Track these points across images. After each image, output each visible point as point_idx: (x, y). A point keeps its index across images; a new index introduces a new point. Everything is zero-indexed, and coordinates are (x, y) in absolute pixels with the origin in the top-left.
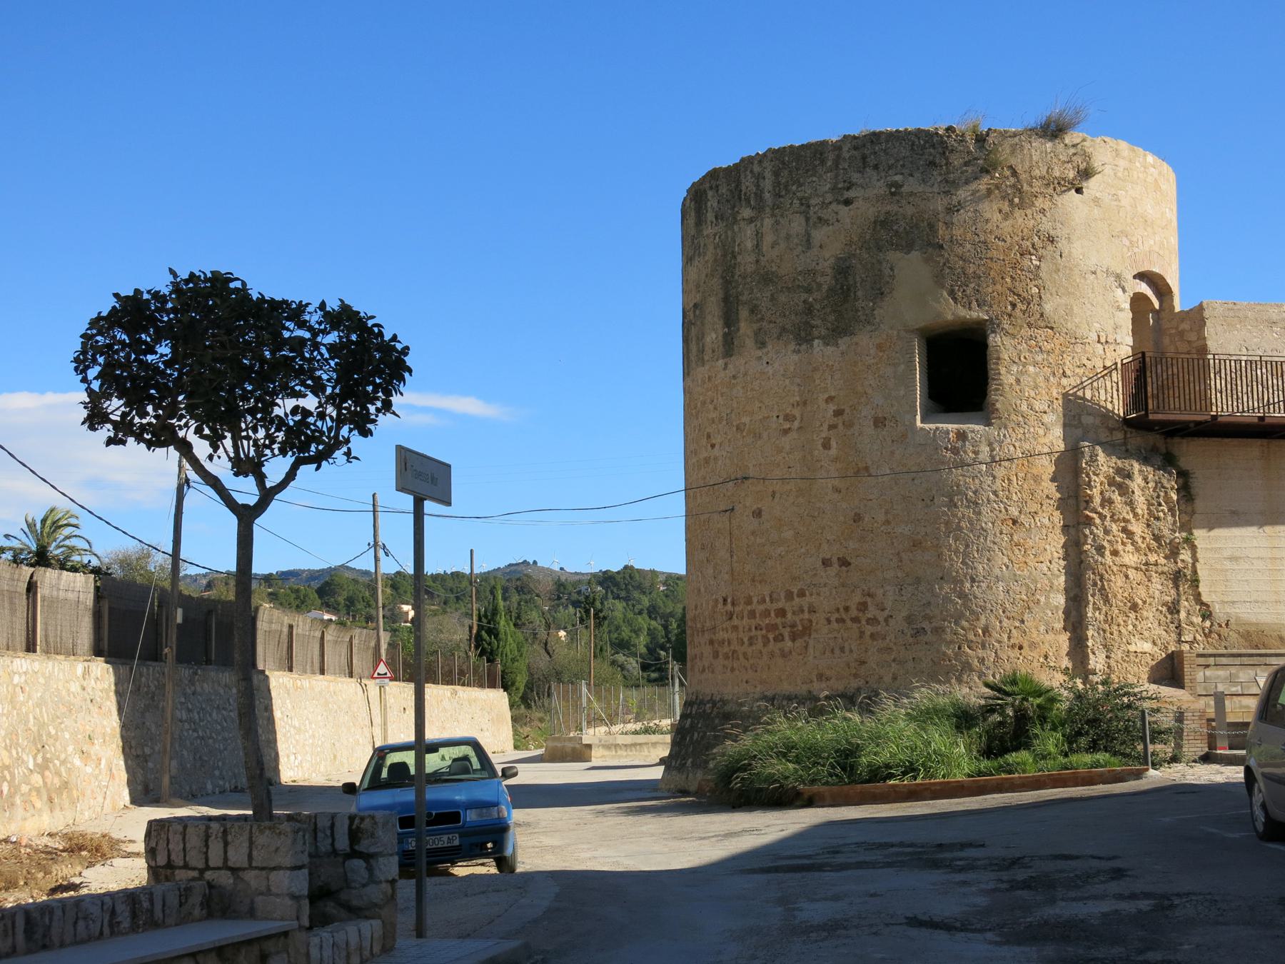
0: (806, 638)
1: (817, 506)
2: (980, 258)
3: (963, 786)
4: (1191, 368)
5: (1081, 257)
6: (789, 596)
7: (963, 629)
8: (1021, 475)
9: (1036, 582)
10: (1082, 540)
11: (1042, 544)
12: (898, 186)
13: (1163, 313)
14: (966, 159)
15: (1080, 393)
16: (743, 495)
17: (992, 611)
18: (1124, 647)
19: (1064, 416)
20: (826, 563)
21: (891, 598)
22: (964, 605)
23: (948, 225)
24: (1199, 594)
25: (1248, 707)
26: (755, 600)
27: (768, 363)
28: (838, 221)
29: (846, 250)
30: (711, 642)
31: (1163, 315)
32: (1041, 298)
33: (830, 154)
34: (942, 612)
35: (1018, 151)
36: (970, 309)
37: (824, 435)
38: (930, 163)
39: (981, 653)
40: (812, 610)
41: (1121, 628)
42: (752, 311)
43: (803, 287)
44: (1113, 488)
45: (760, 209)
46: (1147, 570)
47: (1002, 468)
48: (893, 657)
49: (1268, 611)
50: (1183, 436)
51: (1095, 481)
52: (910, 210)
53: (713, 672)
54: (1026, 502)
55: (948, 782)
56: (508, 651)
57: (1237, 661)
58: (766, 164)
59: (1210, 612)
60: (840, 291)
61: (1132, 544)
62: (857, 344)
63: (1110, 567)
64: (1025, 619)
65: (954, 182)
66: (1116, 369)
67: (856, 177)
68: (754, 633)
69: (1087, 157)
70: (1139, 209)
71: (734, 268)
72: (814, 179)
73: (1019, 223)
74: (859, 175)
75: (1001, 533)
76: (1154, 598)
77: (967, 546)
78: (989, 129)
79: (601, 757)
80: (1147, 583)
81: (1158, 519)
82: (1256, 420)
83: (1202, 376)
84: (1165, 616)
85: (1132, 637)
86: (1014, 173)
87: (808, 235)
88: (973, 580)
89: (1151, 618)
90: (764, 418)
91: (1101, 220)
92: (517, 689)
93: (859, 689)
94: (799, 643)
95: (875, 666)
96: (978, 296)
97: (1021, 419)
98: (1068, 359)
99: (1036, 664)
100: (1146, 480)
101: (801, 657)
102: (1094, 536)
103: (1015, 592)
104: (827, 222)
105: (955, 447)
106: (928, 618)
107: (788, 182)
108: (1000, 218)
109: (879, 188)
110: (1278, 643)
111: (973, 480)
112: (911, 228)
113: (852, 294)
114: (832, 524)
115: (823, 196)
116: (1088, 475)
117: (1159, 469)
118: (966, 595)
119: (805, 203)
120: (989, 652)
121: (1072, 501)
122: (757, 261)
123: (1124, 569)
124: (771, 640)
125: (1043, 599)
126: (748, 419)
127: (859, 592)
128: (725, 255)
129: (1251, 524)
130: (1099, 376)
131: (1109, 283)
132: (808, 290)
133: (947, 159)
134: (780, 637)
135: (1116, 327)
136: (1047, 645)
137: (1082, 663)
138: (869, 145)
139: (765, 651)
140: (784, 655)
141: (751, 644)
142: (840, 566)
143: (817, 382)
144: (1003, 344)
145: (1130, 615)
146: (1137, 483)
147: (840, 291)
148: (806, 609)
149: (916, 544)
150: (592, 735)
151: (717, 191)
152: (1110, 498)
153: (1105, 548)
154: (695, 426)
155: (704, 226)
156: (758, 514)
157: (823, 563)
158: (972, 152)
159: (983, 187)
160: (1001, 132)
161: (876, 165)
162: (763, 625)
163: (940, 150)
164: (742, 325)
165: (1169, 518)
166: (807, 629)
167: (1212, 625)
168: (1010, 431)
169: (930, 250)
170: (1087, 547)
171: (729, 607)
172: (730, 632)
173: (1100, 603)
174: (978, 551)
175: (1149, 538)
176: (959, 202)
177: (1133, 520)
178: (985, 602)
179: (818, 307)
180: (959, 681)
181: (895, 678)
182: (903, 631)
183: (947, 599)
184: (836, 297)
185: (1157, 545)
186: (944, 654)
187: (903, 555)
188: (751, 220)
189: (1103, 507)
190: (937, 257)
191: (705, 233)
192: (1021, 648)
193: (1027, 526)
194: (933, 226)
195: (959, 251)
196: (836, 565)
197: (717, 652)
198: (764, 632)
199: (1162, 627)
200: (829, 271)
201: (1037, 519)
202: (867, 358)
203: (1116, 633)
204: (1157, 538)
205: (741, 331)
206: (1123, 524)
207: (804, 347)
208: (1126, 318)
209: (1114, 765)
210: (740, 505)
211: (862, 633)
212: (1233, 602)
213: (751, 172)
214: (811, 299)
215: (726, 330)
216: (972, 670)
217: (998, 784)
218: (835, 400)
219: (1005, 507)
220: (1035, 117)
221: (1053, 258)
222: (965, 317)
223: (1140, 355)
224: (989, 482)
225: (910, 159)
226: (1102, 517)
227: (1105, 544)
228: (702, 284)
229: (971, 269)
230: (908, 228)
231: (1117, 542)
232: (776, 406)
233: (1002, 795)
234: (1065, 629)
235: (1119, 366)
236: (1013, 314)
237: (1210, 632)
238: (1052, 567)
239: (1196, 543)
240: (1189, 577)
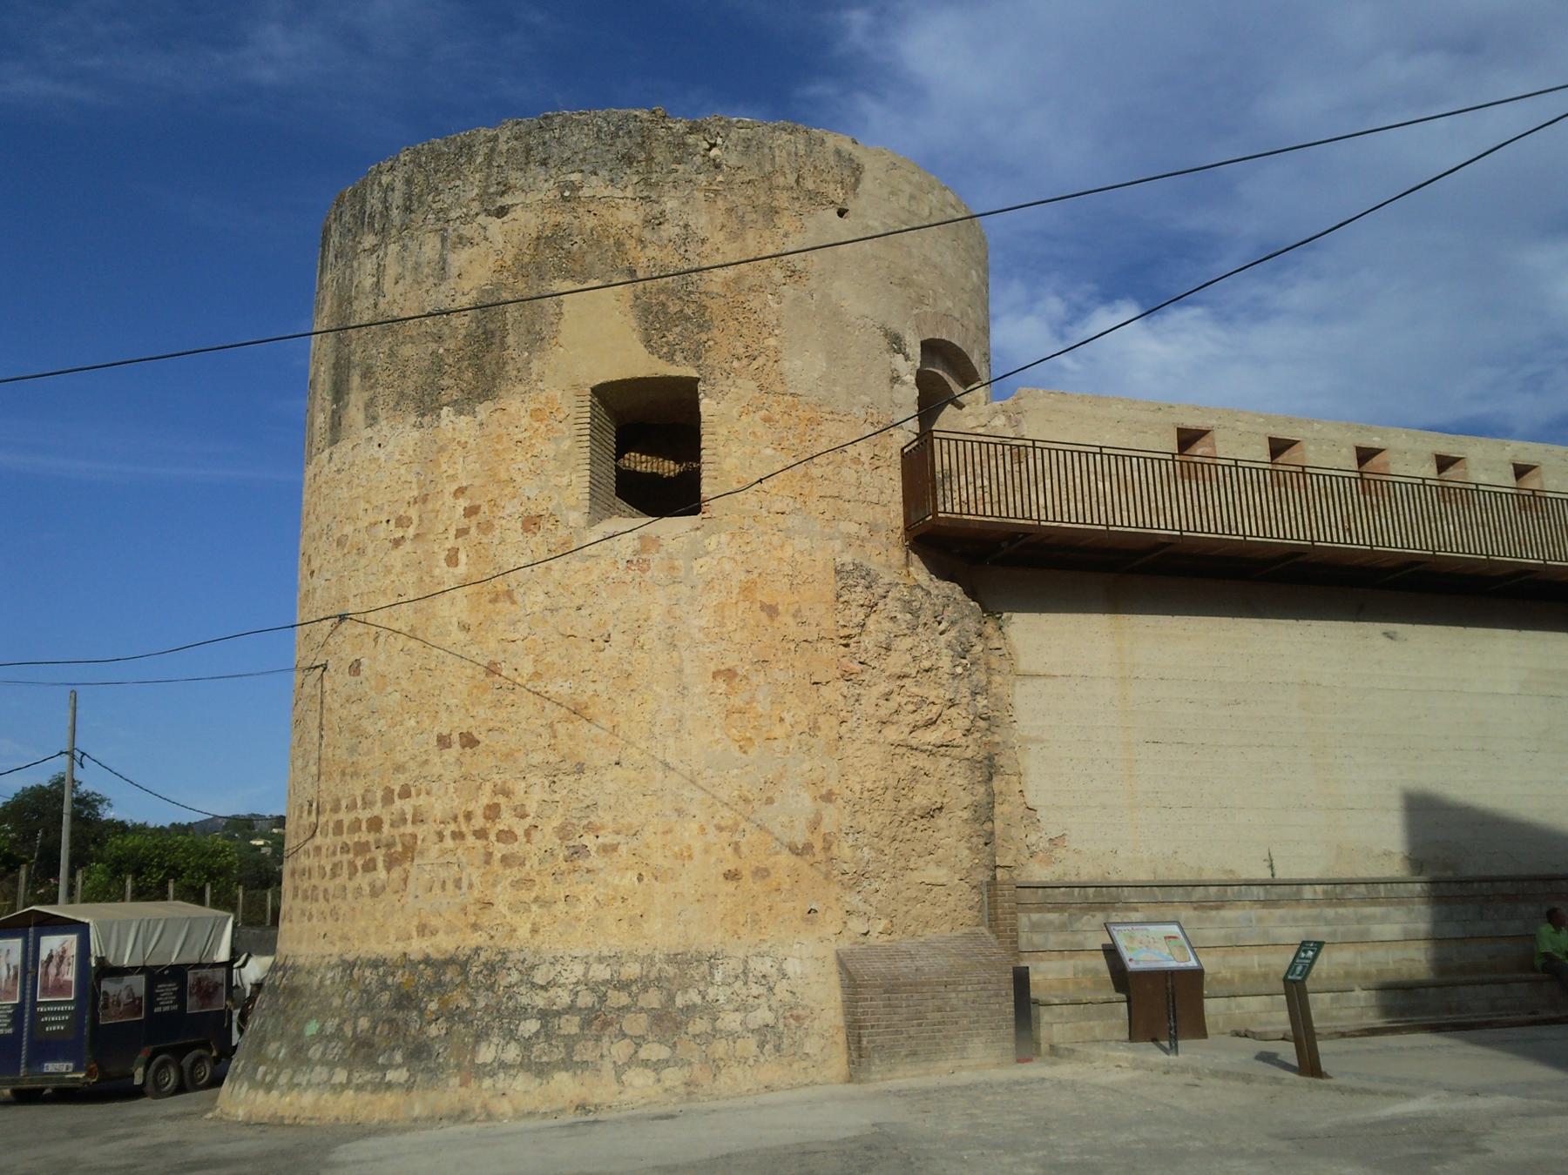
0: (407, 865)
12: (575, 188)
20: (443, 742)
21: (536, 797)
26: (344, 804)
27: (380, 445)
28: (486, 239)
37: (448, 545)
40: (418, 819)
42: (364, 376)
43: (431, 334)
48: (534, 895)
67: (515, 177)
72: (458, 183)
74: (519, 174)
87: (445, 261)
93: (477, 950)
94: (397, 873)
115: (467, 206)
124: (360, 868)
128: (340, 306)
142: (463, 747)
143: (444, 467)
148: (409, 817)
163: (639, 140)
181: (534, 931)
187: (558, 727)
188: (373, 249)
198: (351, 855)
207: (427, 419)
214: (441, 351)
215: (335, 406)
218: (467, 492)
225: (594, 151)
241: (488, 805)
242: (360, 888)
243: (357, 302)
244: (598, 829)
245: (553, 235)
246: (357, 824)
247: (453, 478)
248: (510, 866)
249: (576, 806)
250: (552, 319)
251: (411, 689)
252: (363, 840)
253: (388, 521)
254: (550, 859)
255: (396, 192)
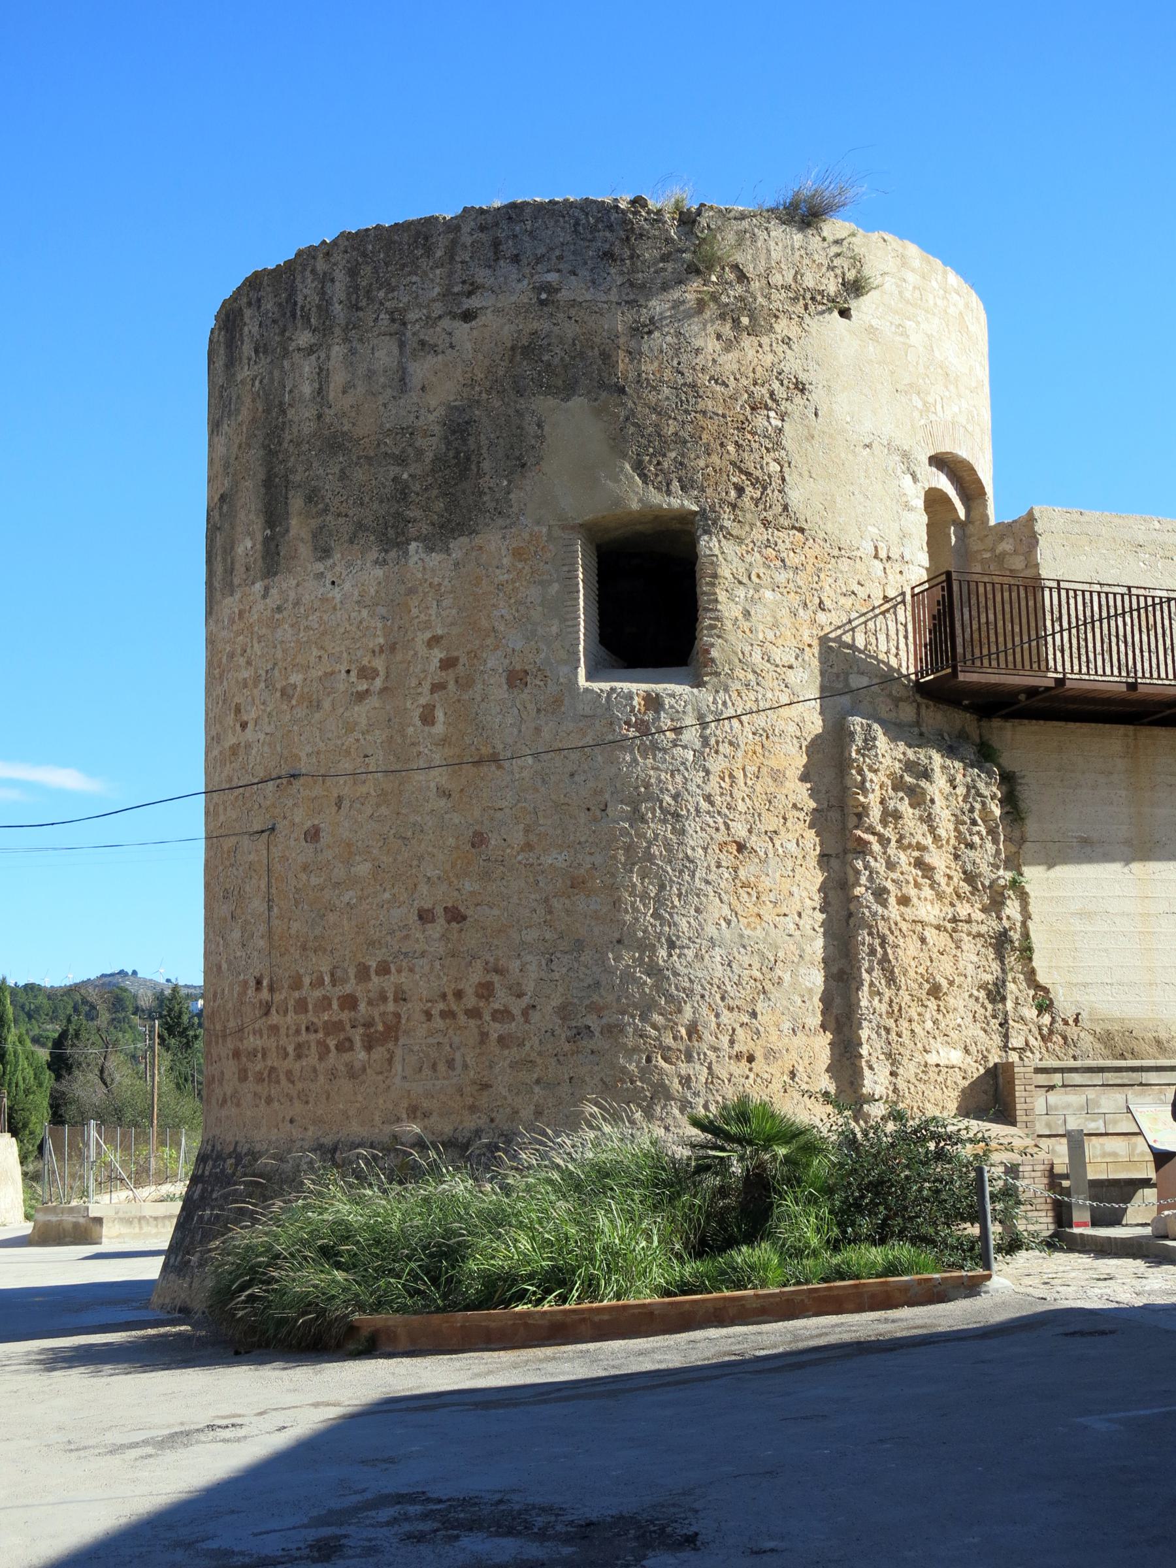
0: (390, 1045)
1: (412, 820)
2: (687, 412)
3: (652, 1313)
4: (1015, 611)
5: (848, 419)
6: (363, 973)
7: (655, 1027)
8: (751, 769)
9: (777, 947)
10: (851, 879)
11: (786, 885)
13: (971, 526)
14: (664, 250)
15: (847, 638)
16: (290, 803)
17: (703, 996)
18: (918, 1057)
19: (822, 673)
20: (425, 916)
21: (534, 976)
22: (657, 987)
23: (634, 355)
24: (1033, 972)
25: (1115, 1154)
26: (307, 981)
27: (333, 583)
28: (452, 347)
29: (465, 395)
30: (237, 1054)
31: (971, 529)
32: (783, 480)
33: (440, 238)
34: (618, 999)
35: (748, 243)
36: (669, 493)
37: (423, 701)
38: (605, 254)
39: (684, 1068)
40: (401, 997)
41: (914, 1025)
42: (309, 499)
43: (393, 456)
44: (901, 794)
45: (324, 330)
46: (955, 930)
47: (721, 757)
48: (535, 1076)
49: (1138, 999)
50: (1007, 717)
51: (872, 781)
52: (570, 330)
53: (238, 1105)
54: (760, 815)
55: (625, 1307)
56: (20, 1078)
57: (1098, 1079)
58: (337, 257)
59: (1051, 1000)
60: (454, 462)
61: (932, 887)
62: (481, 548)
63: (896, 924)
64: (758, 1010)
65: (643, 286)
66: (903, 602)
67: (482, 275)
68: (304, 1036)
69: (856, 261)
70: (937, 353)
71: (283, 430)
72: (414, 279)
73: (750, 357)
74: (488, 272)
75: (718, 867)
76: (965, 976)
77: (662, 887)
78: (702, 205)
79: (117, 1237)
80: (954, 951)
81: (971, 846)
82: (1124, 688)
83: (1033, 624)
84: (983, 1006)
85: (932, 1041)
86: (742, 277)
87: (404, 370)
88: (672, 945)
89: (961, 1010)
90: (326, 674)
91: (879, 363)
92: (31, 1133)
93: (478, 1133)
94: (379, 1053)
95: (504, 1092)
96: (682, 473)
97: (751, 676)
98: (826, 582)
99: (776, 1086)
100: (952, 782)
101: (380, 1077)
102: (871, 873)
103: (741, 965)
104: (434, 350)
105: (642, 721)
106: (596, 1009)
107: (371, 284)
108: (718, 348)
109: (520, 292)
110: (1153, 1050)
111: (672, 776)
112: (573, 358)
113: (473, 467)
114: (435, 851)
116: (860, 771)
117: (972, 767)
118: (661, 970)
119: (398, 318)
120: (698, 1067)
121: (834, 815)
122: (319, 417)
123: (919, 928)
124: (333, 1048)
125: (787, 977)
126: (301, 676)
127: (479, 965)
128: (268, 411)
129: (1108, 858)
130: (877, 611)
131: (892, 464)
132: (401, 461)
133: (632, 249)
134: (347, 1044)
135: (904, 536)
136: (794, 1053)
137: (852, 1083)
138: (504, 224)
139: (321, 1067)
140: (353, 1074)
141: (299, 1057)
142: (449, 922)
143: (415, 612)
144: (723, 553)
145: (928, 1003)
146: (937, 787)
147: (454, 462)
149: (576, 884)
150: (102, 1204)
151: (259, 307)
152: (896, 810)
153: (889, 892)
154: (218, 696)
155: (238, 368)
156: (313, 835)
157: (421, 917)
158: (673, 240)
159: (691, 297)
160: (720, 211)
161: (517, 256)
162: (320, 1024)
163: (622, 234)
164: (294, 522)
165: (989, 845)
166: (392, 1031)
167: (1053, 1021)
168: (734, 695)
169: (604, 394)
170: (858, 891)
171: (265, 994)
172: (265, 1037)
173: (882, 985)
174: (679, 895)
175: (957, 876)
176: (652, 319)
177: (932, 847)
178: (691, 981)
179: (417, 487)
180: (649, 1115)
182: (553, 1032)
183: (628, 977)
184: (446, 472)
185: (970, 888)
186: (623, 1070)
187: (555, 902)
188: (311, 350)
189: (885, 825)
190: (615, 406)
191: (239, 378)
192: (751, 1059)
193: (762, 854)
194: (609, 357)
195: (652, 398)
196: (442, 921)
197: (246, 1071)
198: (320, 1035)
199: (978, 1025)
200: (437, 429)
201: (778, 843)
202: (498, 571)
203: (906, 1034)
204: (970, 878)
205: (292, 533)
206: (916, 854)
207: (393, 554)
208: (919, 521)
209: (925, 1268)
210: (286, 822)
211: (484, 1036)
212: (1085, 985)
213: (313, 271)
214: (405, 476)
215: (268, 532)
216: (669, 1097)
217: (716, 1309)
219: (725, 823)
220: (776, 194)
221: (803, 416)
222: (661, 507)
223: (944, 577)
224: (700, 781)
225: (572, 247)
226: (884, 841)
227: (889, 885)
228: (232, 461)
229: (671, 428)
230: (567, 358)
231: (908, 882)
232: (345, 655)
233: (724, 1331)
234: (824, 1027)
235: (908, 598)
236: (740, 504)
237: (1051, 1032)
238: (801, 923)
239: (1028, 888)
240: (1017, 944)
241: (480, 983)
242: (334, 1068)
243: (293, 411)
244: (602, 1009)
245: (530, 343)
246: (326, 1002)
247: (428, 625)
248: (508, 1047)
249: (576, 985)
250: (533, 442)
251: (385, 859)
252: (335, 1019)
253: (348, 672)
254: (552, 1039)
255: (337, 283)
